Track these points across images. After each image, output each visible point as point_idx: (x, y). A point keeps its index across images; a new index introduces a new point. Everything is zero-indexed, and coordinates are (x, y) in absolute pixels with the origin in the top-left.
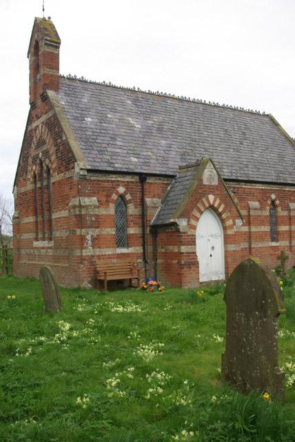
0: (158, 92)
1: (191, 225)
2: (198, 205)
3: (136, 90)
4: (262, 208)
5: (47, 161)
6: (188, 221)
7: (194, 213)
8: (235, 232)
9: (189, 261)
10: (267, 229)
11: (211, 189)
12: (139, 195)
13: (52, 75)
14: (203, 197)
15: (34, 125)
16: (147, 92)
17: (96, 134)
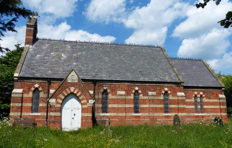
0: (90, 41)
2: (63, 92)
3: (78, 41)
6: (56, 100)
7: (60, 96)
10: (132, 106)
12: (47, 88)
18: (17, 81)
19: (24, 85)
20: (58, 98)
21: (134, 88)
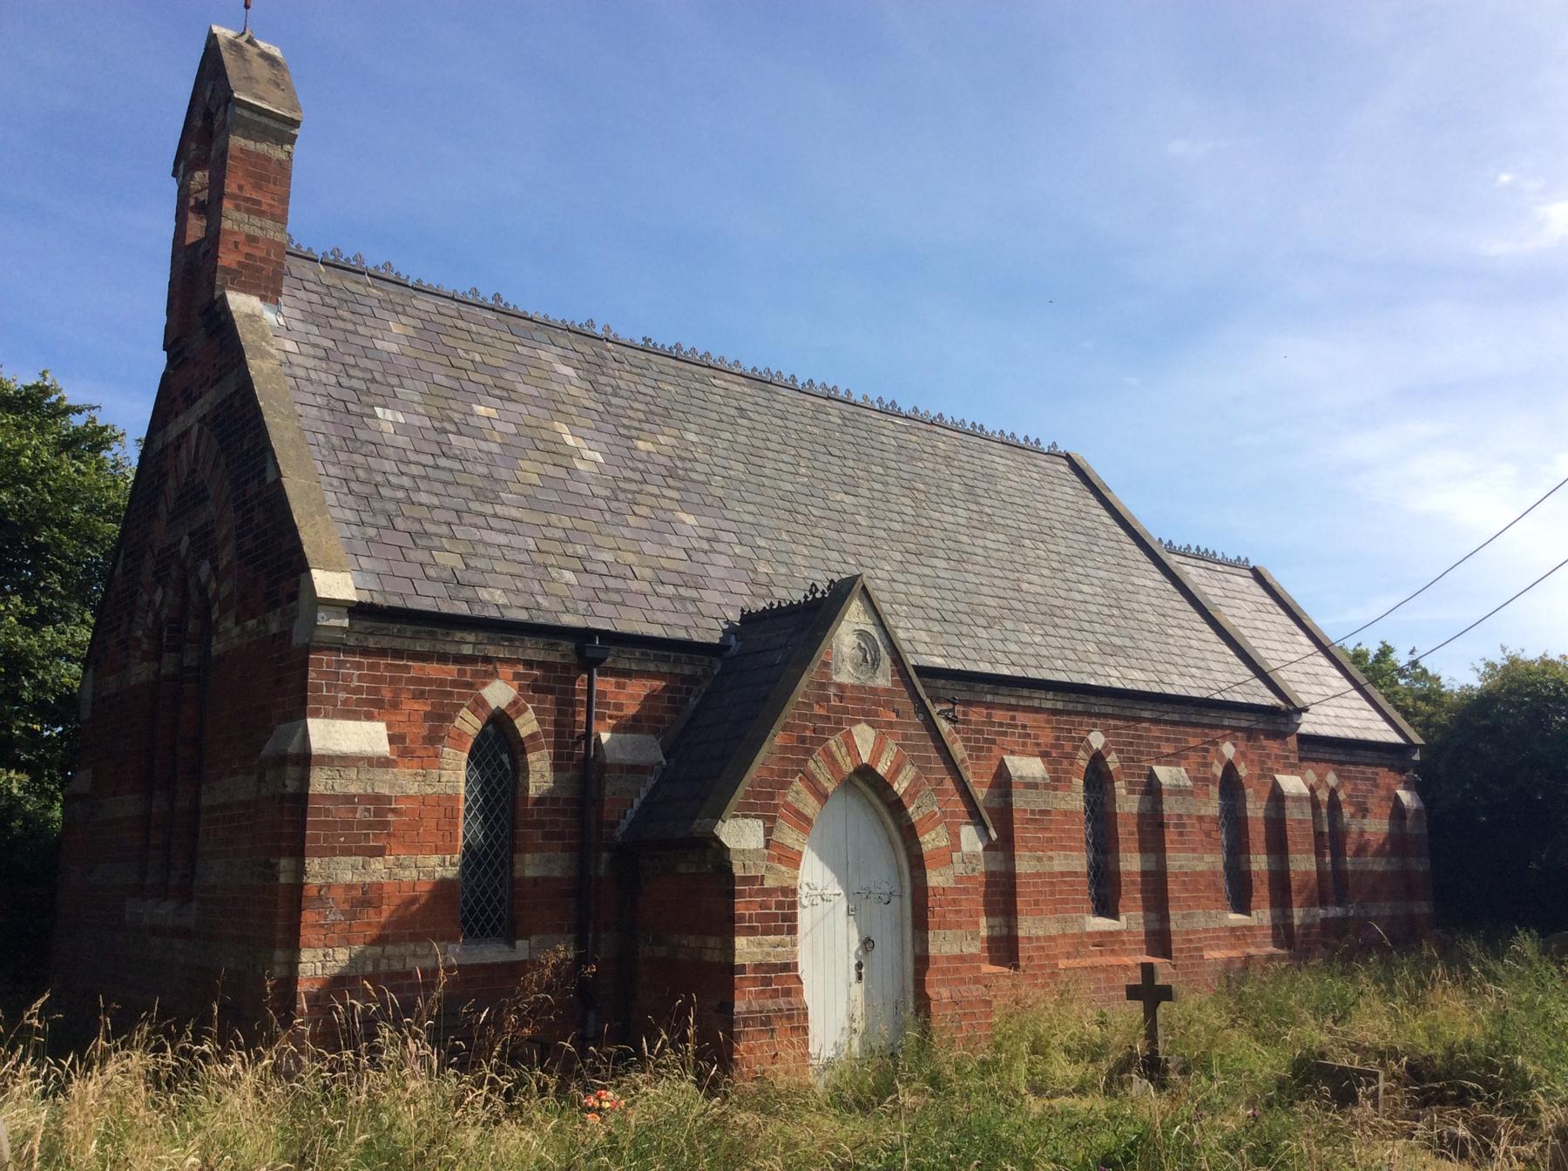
1: (781, 846)
4: (1057, 780)
5: (205, 568)
6: (768, 832)
8: (958, 879)
9: (770, 1004)
11: (864, 704)
13: (252, 239)
14: (833, 731)
15: (174, 430)
16: (640, 342)
17: (414, 470)
18: (336, 646)
19: (393, 680)
20: (782, 817)
21: (1083, 734)
